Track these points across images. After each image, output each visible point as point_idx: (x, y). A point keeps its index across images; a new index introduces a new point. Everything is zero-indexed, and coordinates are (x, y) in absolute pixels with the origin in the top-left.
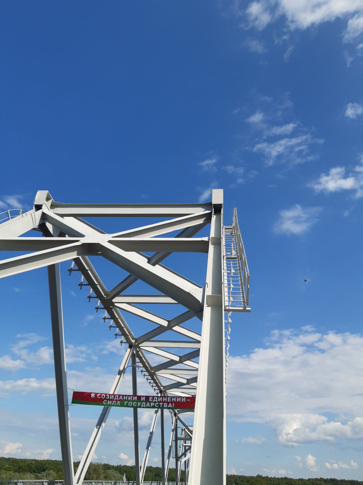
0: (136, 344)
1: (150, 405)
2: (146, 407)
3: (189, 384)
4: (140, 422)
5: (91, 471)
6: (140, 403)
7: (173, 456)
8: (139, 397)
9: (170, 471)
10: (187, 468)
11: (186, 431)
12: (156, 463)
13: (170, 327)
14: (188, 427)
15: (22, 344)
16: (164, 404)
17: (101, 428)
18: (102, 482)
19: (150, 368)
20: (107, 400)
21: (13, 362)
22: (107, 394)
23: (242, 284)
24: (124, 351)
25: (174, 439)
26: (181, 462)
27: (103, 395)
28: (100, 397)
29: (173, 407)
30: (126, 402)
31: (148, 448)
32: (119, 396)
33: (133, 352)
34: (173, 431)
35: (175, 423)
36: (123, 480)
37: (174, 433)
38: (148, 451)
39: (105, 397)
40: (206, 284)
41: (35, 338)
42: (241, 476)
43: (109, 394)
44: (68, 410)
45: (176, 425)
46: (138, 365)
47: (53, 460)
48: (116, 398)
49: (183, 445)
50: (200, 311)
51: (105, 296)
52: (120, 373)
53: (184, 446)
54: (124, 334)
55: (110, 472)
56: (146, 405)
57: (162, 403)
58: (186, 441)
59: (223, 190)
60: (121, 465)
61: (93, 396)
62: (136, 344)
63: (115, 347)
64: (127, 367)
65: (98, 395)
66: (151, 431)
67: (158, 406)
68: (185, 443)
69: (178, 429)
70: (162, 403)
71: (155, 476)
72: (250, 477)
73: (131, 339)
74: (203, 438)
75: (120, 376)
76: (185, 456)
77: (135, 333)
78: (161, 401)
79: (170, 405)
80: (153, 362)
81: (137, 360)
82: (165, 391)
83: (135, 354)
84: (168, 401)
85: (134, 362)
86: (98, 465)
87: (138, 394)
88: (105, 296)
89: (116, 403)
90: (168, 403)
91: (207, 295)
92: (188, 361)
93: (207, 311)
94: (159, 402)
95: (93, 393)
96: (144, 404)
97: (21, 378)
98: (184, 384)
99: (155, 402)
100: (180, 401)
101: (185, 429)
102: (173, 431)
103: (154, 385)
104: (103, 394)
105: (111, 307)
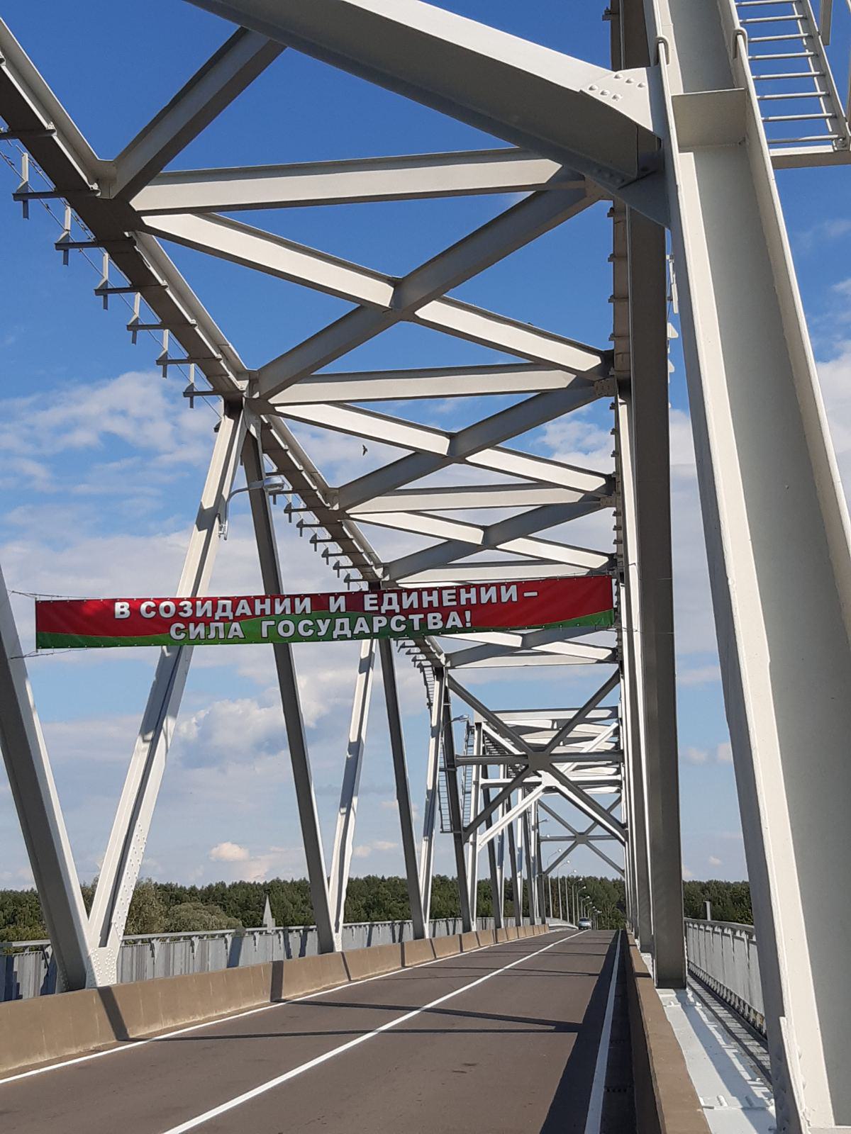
0: (256, 395)
1: (371, 627)
6: (328, 621)
7: (442, 827)
10: (498, 867)
11: (484, 732)
13: (402, 309)
14: (496, 715)
16: (430, 616)
18: (190, 937)
19: (324, 495)
20: (186, 621)
22: (182, 600)
23: (810, 37)
25: (441, 764)
26: (474, 844)
27: (163, 604)
28: (153, 614)
29: (468, 625)
30: (265, 624)
32: (236, 601)
33: (248, 431)
34: (435, 732)
36: (266, 926)
37: (442, 740)
40: (661, 46)
42: (710, 883)
44: (24, 675)
45: (447, 709)
49: (477, 783)
51: (95, 187)
52: (206, 520)
53: (483, 786)
54: (198, 355)
55: (184, 910)
57: (422, 616)
60: (223, 884)
61: (122, 613)
62: (256, 395)
64: (230, 496)
65: (144, 606)
66: (354, 739)
67: (403, 627)
68: (485, 776)
70: (422, 616)
71: (363, 911)
73: (231, 376)
75: (205, 532)
76: (489, 825)
78: (416, 606)
81: (268, 464)
84: (446, 603)
85: (254, 471)
89: (227, 631)
95: (121, 600)
96: (342, 624)
98: (473, 548)
99: (390, 614)
100: (494, 600)
101: (479, 725)
103: (346, 561)
104: (166, 600)
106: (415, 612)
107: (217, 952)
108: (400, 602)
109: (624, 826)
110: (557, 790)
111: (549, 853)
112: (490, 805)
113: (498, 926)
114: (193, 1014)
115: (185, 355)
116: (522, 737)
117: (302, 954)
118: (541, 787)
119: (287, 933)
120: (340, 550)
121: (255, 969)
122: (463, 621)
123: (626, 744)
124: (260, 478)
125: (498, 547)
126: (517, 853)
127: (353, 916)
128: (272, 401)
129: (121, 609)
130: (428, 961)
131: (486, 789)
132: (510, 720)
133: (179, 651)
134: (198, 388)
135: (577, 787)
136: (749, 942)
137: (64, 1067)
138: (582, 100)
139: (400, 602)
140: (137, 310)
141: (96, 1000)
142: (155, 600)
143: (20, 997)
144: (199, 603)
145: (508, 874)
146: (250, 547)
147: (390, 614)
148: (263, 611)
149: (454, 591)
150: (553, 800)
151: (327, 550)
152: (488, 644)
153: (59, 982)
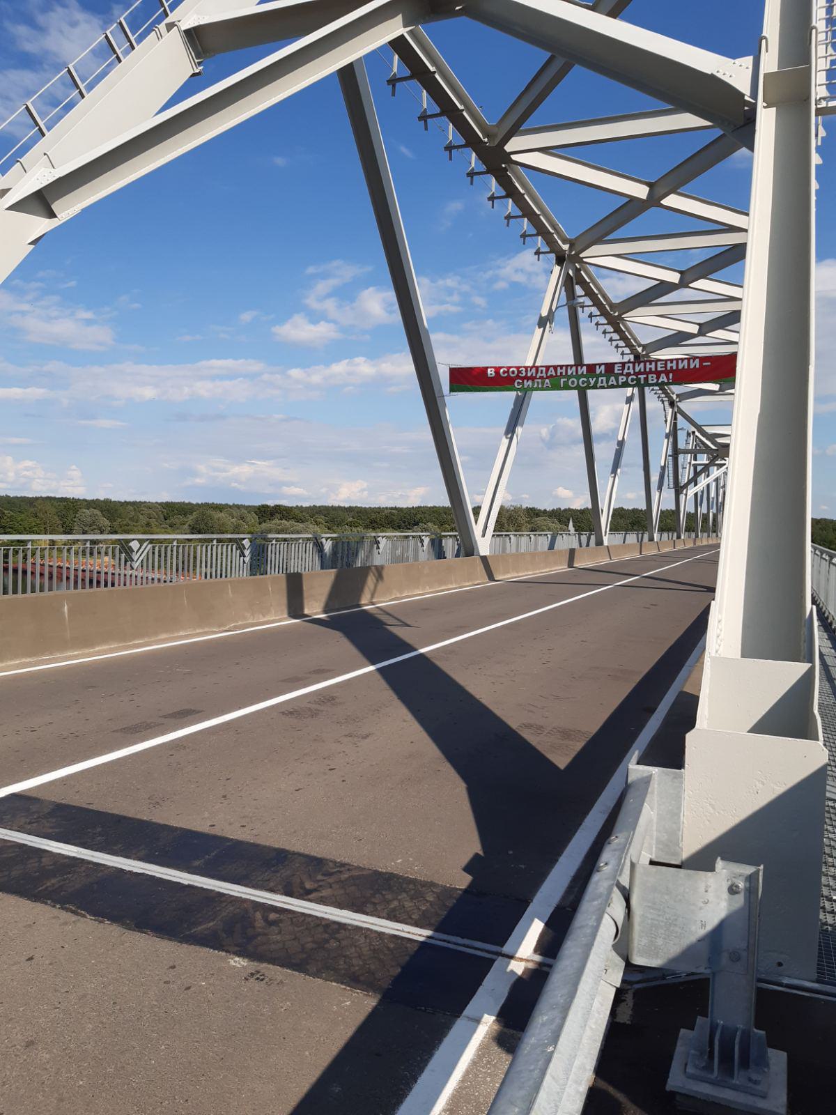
0: (573, 253)
1: (617, 381)
2: (609, 387)
3: (704, 335)
4: (596, 427)
5: (504, 520)
6: (595, 379)
8: (591, 368)
9: (664, 515)
11: (696, 436)
12: (633, 499)
13: (654, 200)
15: (322, 287)
16: (650, 376)
17: (515, 437)
20: (523, 379)
21: (311, 327)
22: (521, 367)
24: (542, 279)
25: (670, 452)
26: (686, 495)
27: (511, 370)
28: (506, 375)
29: (671, 381)
30: (562, 380)
31: (614, 471)
32: (548, 368)
33: (568, 273)
34: (667, 436)
35: (671, 421)
36: (569, 531)
37: (671, 440)
38: (615, 477)
39: (516, 372)
40: (764, 41)
41: (346, 271)
42: (821, 519)
43: (524, 367)
44: (445, 405)
45: (675, 424)
46: (582, 301)
47: (429, 506)
48: (542, 373)
49: (690, 463)
50: (744, 126)
51: (486, 140)
52: (542, 323)
53: (693, 465)
56: (607, 382)
57: (645, 376)
58: (698, 455)
60: (560, 509)
61: (491, 374)
62: (573, 253)
63: (522, 270)
64: (556, 309)
65: (502, 371)
67: (635, 382)
68: (695, 460)
69: (679, 432)
70: (645, 376)
73: (560, 242)
74: (759, 411)
75: (542, 329)
76: (696, 485)
77: (567, 227)
78: (642, 370)
79: (663, 378)
80: (617, 291)
81: (579, 290)
83: (572, 278)
84: (659, 369)
85: (571, 295)
86: (517, 510)
87: (586, 361)
88: (486, 140)
89: (543, 384)
90: (658, 374)
91: (766, 72)
92: (702, 281)
93: (766, 121)
94: (636, 374)
95: (491, 367)
96: (602, 380)
97: (337, 360)
98: (692, 336)
99: (628, 375)
101: (694, 433)
102: (667, 436)
103: (622, 343)
105: (503, 166)
107: (543, 542)
108: (634, 369)
112: (697, 474)
113: (697, 536)
114: (527, 570)
115: (535, 232)
116: (716, 439)
117: (588, 545)
119: (580, 535)
120: (618, 338)
121: (560, 552)
122: (668, 379)
124: (574, 298)
126: (711, 500)
127: (614, 528)
128: (581, 256)
129: (491, 372)
130: (655, 552)
131: (695, 466)
132: (710, 430)
133: (526, 391)
134: (542, 250)
138: (712, 79)
139: (634, 369)
140: (510, 208)
141: (479, 561)
142: (507, 367)
143: (445, 558)
144: (529, 369)
145: (704, 510)
146: (566, 337)
148: (561, 373)
149: (664, 362)
151: (611, 338)
152: (700, 389)
153: (462, 552)
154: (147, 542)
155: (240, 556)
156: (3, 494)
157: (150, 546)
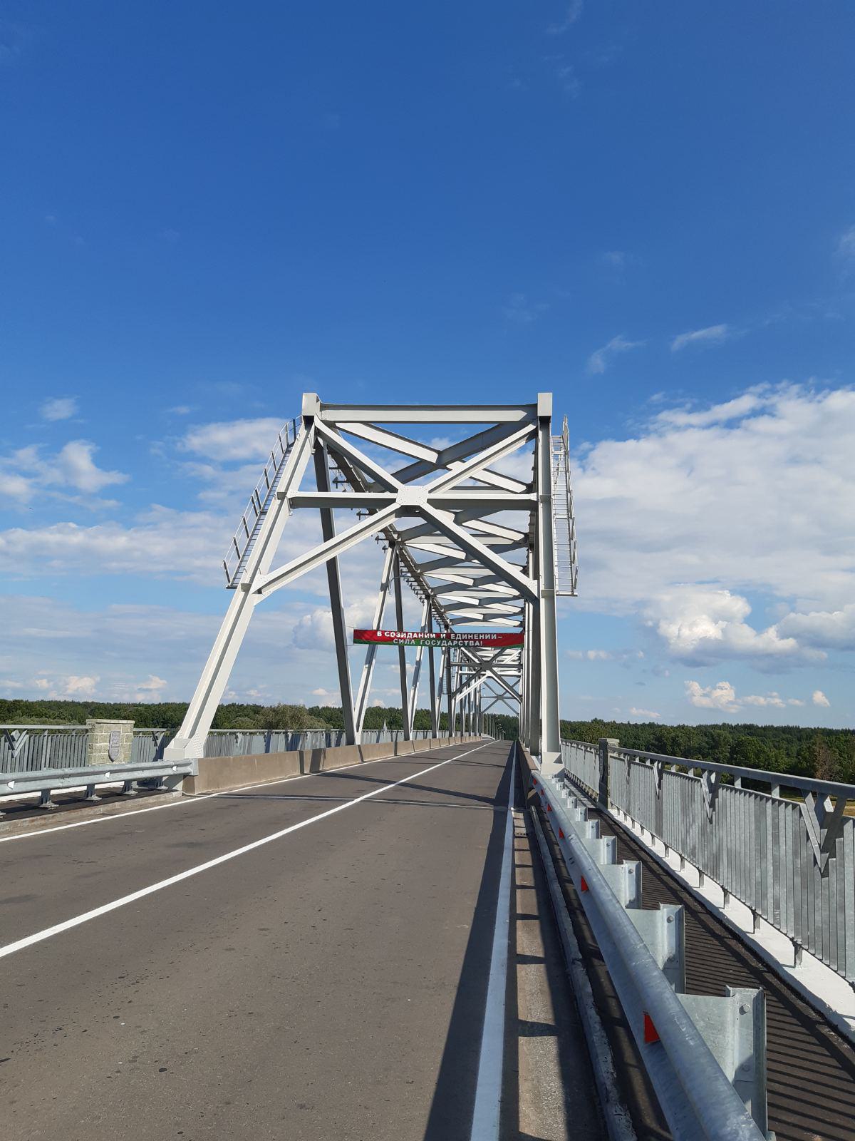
9: (420, 714)
12: (388, 698)
26: (455, 699)
37: (447, 656)
49: (457, 673)
59: (551, 394)
60: (318, 707)
68: (461, 670)
72: (578, 722)
79: (477, 643)
82: (403, 543)
89: (410, 642)
90: (475, 641)
98: (461, 561)
99: (458, 640)
106: (466, 640)
109: (521, 696)
110: (492, 677)
111: (485, 704)
114: (377, 756)
117: (338, 744)
118: (485, 676)
123: (524, 661)
125: (463, 524)
127: (367, 727)
134: (340, 479)
135: (499, 677)
136: (595, 754)
137: (160, 809)
145: (467, 712)
147: (458, 640)
150: (490, 682)
154: (26, 732)
155: (9, 749)
156: (1, 698)
157: (28, 736)
